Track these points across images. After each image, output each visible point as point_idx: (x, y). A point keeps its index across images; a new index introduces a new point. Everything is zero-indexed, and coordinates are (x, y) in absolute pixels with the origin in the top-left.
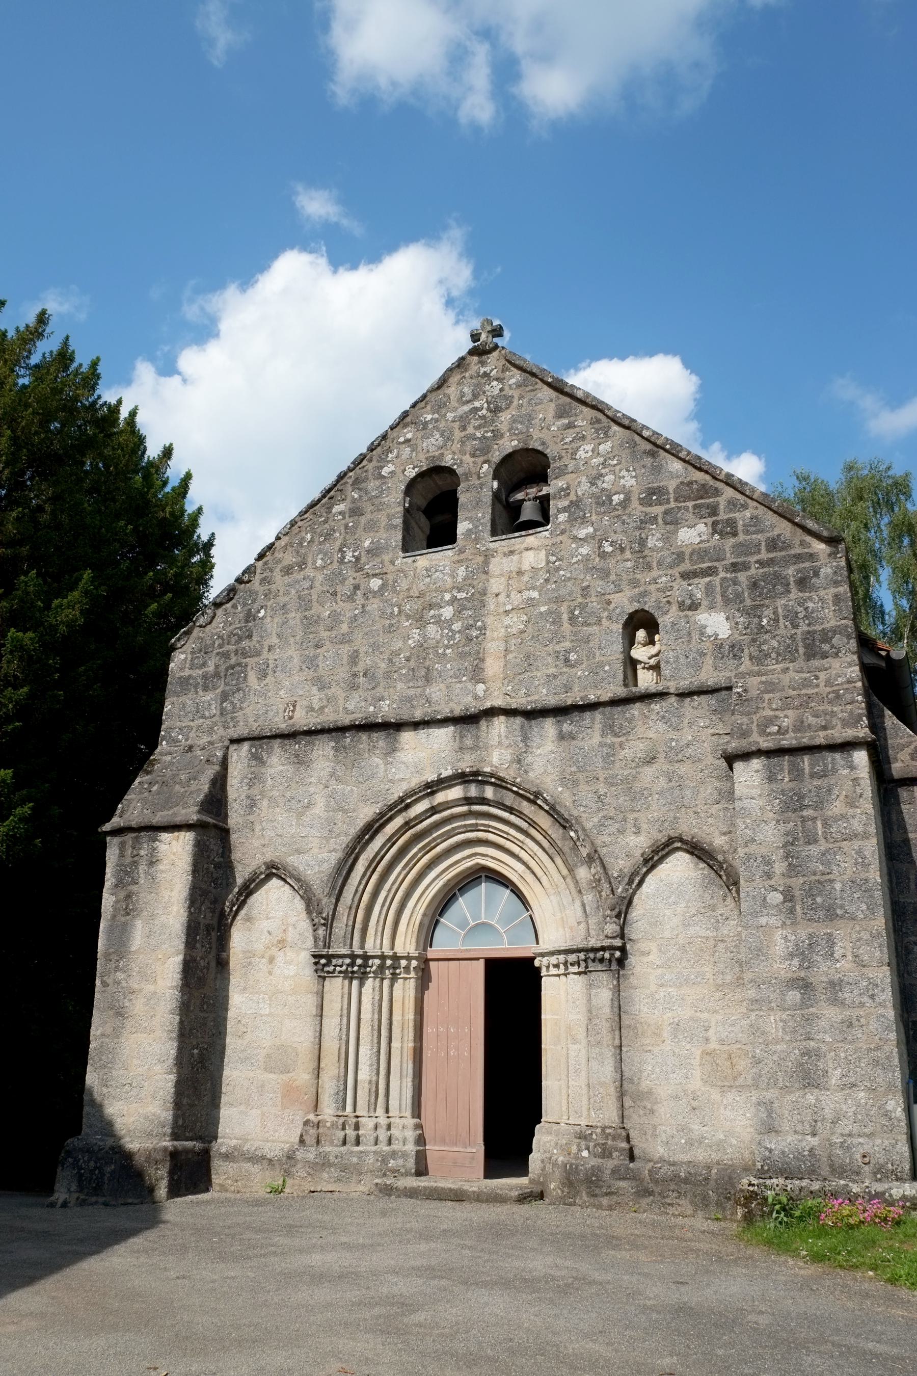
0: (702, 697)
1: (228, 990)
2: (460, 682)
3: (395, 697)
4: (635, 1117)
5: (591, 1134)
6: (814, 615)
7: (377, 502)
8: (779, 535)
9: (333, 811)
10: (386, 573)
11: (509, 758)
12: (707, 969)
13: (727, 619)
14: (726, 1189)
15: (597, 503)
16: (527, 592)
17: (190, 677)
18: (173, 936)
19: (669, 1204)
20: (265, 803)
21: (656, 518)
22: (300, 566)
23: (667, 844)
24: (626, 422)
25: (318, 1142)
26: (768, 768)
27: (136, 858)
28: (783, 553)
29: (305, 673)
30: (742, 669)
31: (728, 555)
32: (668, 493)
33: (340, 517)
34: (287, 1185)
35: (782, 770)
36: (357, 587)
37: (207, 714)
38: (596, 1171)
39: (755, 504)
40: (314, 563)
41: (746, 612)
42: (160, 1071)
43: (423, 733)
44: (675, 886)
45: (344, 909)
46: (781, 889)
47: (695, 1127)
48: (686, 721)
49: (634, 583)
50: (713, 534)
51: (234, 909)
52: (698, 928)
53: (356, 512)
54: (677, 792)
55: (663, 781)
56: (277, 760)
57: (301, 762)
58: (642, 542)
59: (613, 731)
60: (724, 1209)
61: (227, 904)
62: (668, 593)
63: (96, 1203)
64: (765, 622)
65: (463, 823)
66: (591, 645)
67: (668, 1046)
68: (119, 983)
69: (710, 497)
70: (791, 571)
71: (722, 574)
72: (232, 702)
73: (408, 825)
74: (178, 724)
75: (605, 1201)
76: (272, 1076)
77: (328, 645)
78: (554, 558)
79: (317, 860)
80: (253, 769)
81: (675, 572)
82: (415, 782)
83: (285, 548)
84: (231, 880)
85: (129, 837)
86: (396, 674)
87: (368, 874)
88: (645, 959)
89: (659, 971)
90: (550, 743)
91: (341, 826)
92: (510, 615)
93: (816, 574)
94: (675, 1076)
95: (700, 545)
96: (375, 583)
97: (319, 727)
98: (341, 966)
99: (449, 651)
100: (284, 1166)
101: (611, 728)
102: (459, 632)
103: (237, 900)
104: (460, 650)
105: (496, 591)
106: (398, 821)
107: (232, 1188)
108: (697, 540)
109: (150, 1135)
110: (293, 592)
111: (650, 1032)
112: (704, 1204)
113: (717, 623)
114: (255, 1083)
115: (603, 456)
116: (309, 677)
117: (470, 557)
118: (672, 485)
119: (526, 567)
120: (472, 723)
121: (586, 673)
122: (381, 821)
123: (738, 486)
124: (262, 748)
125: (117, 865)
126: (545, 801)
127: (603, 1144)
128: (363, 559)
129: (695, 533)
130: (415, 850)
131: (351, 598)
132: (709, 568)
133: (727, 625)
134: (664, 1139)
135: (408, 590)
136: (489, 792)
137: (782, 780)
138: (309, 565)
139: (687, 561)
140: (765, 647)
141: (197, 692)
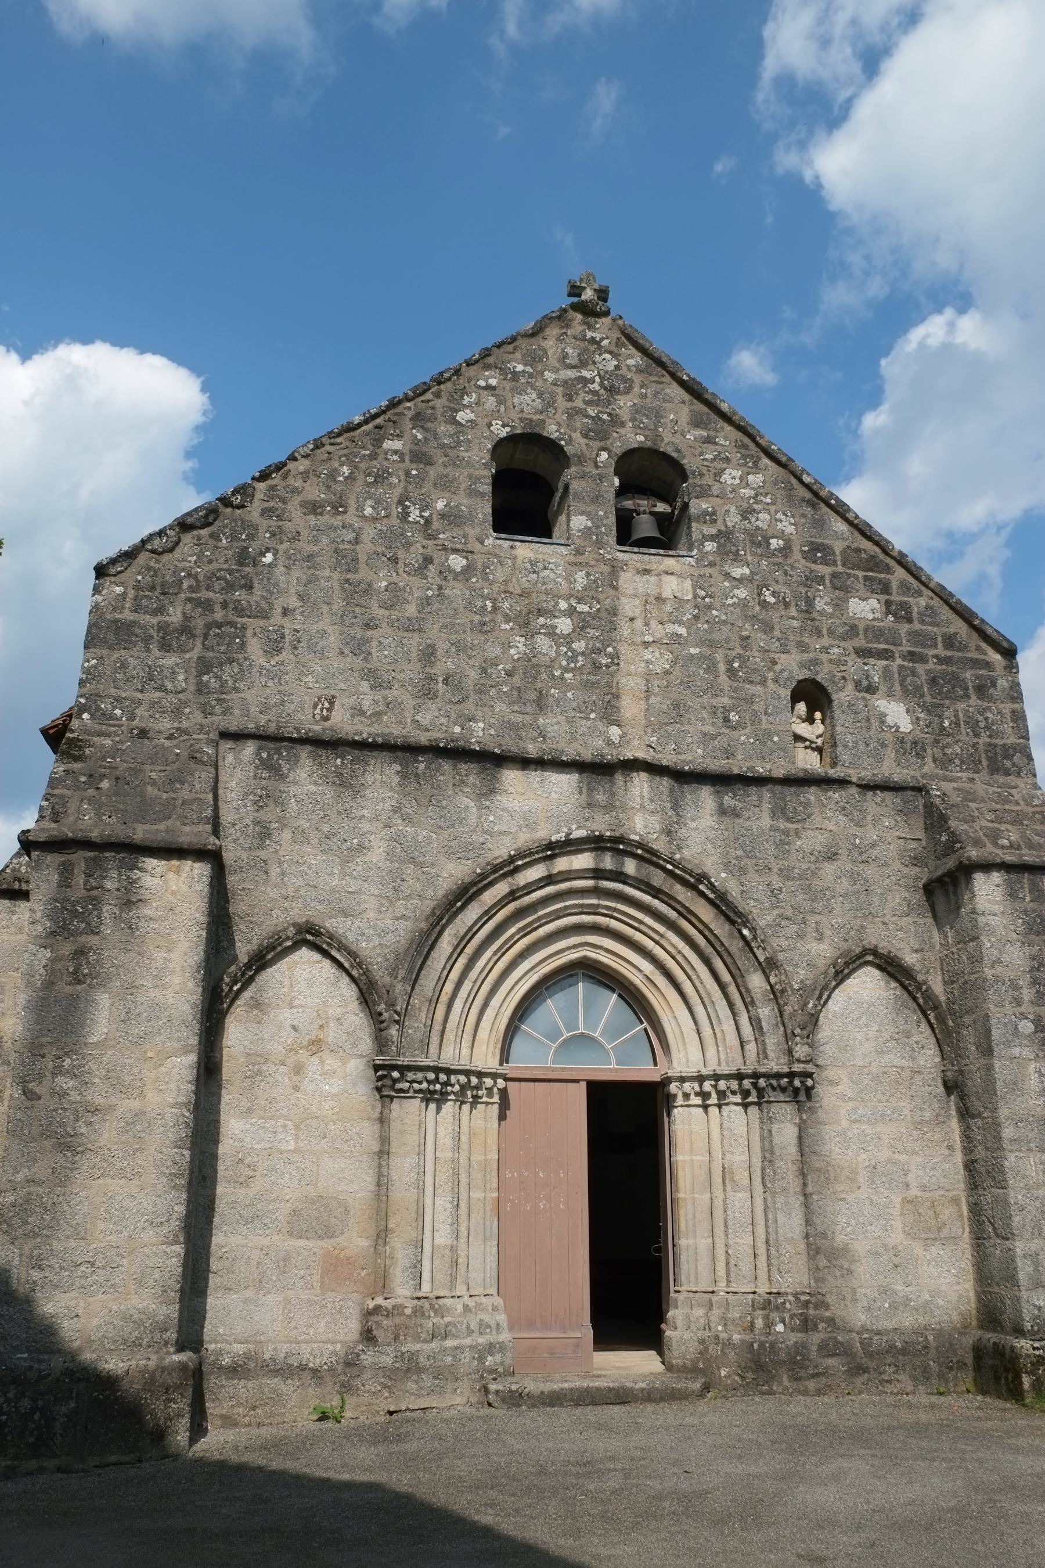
0: (886, 793)
1: (218, 1112)
2: (588, 719)
3: (493, 720)
4: (830, 1279)
5: (784, 1303)
6: (994, 727)
7: (452, 453)
8: (955, 634)
9: (400, 861)
10: (472, 552)
11: (658, 827)
12: (903, 1104)
13: (908, 711)
14: (948, 1357)
15: (753, 542)
16: (672, 626)
17: (133, 624)
18: (175, 1023)
19: (887, 1381)
20: (286, 835)
21: (822, 577)
22: (335, 508)
23: (859, 957)
24: (784, 459)
25: (396, 1338)
26: (1009, 884)
27: (95, 893)
28: (960, 654)
29: (348, 659)
30: (926, 770)
31: (904, 641)
32: (834, 554)
33: (395, 458)
34: (347, 1406)
35: (1022, 888)
36: (428, 560)
37: (169, 685)
38: (801, 1348)
39: (930, 593)
40: (360, 508)
41: (925, 708)
42: (154, 1240)
43: (535, 776)
44: (865, 1006)
45: (422, 1002)
46: (1031, 1017)
47: (899, 1288)
48: (869, 817)
49: (803, 647)
50: (887, 614)
51: (235, 988)
52: (892, 1056)
53: (420, 457)
54: (863, 897)
55: (845, 884)
56: (305, 778)
57: (344, 784)
58: (810, 602)
59: (785, 814)
60: (947, 1381)
61: (227, 980)
62: (843, 668)
63: (41, 1470)
64: (946, 724)
65: (581, 902)
66: (755, 707)
67: (864, 1193)
68: (63, 1094)
69: (880, 572)
70: (968, 675)
71: (899, 661)
72: (218, 678)
73: (512, 895)
74: (113, 691)
75: (812, 1385)
76: (302, 1243)
77: (385, 629)
78: (703, 593)
79: (377, 929)
80: (264, 782)
81: (849, 645)
82: (524, 839)
83: (305, 475)
84: (225, 944)
85: (80, 858)
86: (493, 690)
87: (455, 955)
88: (834, 1090)
89: (851, 1105)
90: (708, 817)
91: (413, 882)
92: (651, 649)
93: (994, 685)
94: (873, 1228)
95: (875, 623)
96: (457, 562)
97: (380, 740)
98: (420, 1083)
99: (567, 675)
100: (342, 1378)
101: (783, 811)
102: (582, 654)
103: (243, 975)
104: (585, 677)
105: (630, 614)
106: (501, 889)
107: (247, 1420)
108: (871, 616)
109: (136, 1344)
110: (325, 540)
111: (843, 1178)
112: (924, 1377)
113: (898, 714)
114: (272, 1254)
115: (752, 488)
116: (356, 667)
117: (593, 563)
118: (838, 547)
119: (667, 593)
120: (603, 774)
121: (752, 740)
122: (480, 885)
123: (913, 568)
124: (280, 754)
125: (56, 900)
126: (712, 887)
127: (801, 1314)
128: (436, 525)
129: (868, 608)
130: (513, 930)
131: (420, 571)
132: (886, 651)
133: (908, 719)
134: (865, 1304)
135: (506, 582)
136: (630, 867)
137: (1024, 899)
138: (352, 509)
139: (861, 637)
140: (948, 751)
141: (148, 650)
